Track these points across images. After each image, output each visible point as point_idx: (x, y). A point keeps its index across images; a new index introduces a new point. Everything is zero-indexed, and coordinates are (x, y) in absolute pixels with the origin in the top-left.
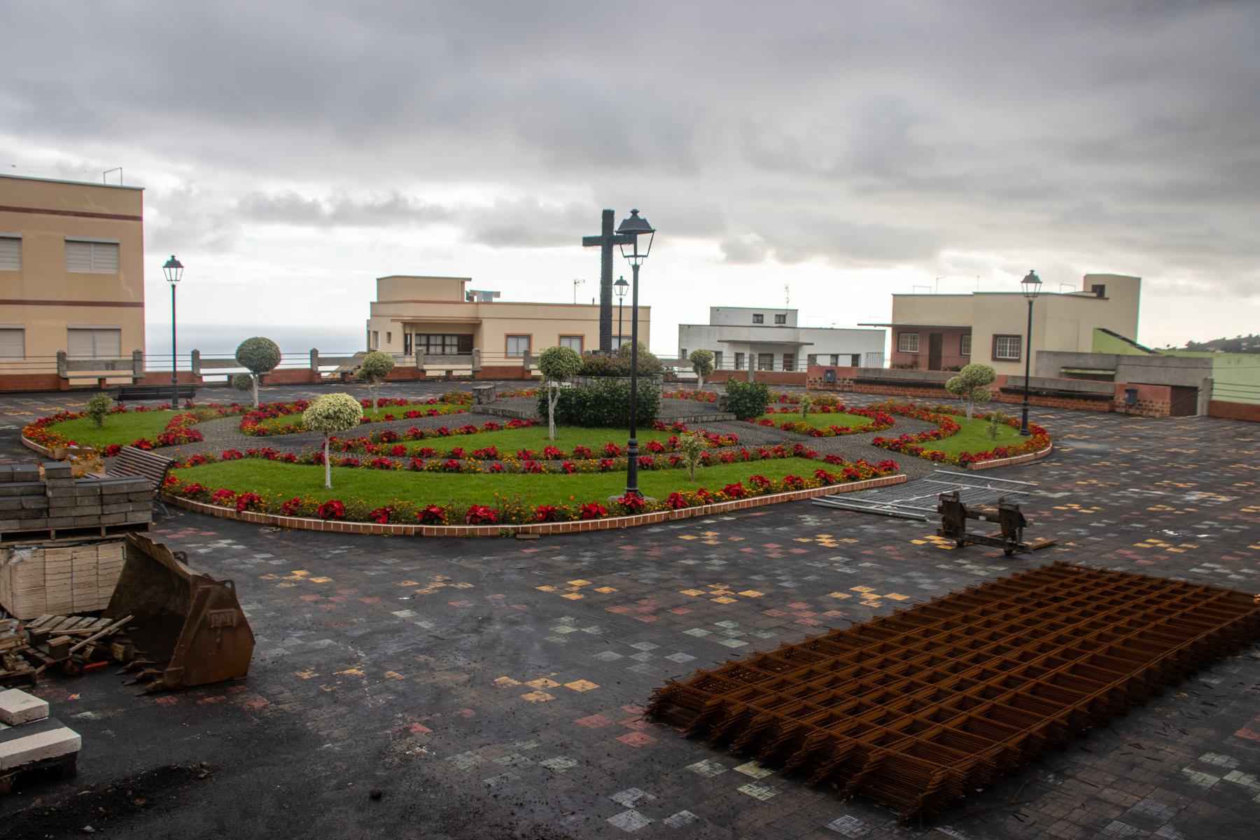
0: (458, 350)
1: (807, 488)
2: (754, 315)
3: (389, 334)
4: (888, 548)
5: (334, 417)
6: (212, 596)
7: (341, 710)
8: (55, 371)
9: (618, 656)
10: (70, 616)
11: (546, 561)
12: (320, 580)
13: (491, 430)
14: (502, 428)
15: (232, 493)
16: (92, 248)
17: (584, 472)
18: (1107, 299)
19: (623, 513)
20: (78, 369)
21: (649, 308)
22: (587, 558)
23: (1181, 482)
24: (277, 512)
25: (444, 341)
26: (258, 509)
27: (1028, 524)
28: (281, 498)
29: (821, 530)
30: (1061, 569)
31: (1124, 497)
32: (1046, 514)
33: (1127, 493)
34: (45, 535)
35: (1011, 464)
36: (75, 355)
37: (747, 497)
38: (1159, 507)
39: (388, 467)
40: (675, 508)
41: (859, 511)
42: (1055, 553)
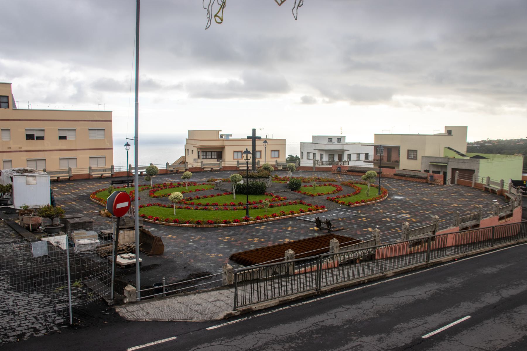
0: (217, 157)
2: (329, 139)
3: (193, 151)
5: (176, 198)
6: (158, 239)
7: (179, 258)
8: (88, 173)
9: (229, 251)
10: (131, 243)
11: (223, 233)
12: (174, 237)
13: (219, 196)
14: (222, 195)
15: (152, 217)
16: (97, 131)
18: (452, 135)
20: (95, 172)
21: (285, 140)
22: (232, 232)
24: (163, 222)
25: (212, 154)
26: (159, 221)
28: (164, 218)
34: (125, 229)
35: (365, 205)
36: (94, 167)
39: (189, 209)
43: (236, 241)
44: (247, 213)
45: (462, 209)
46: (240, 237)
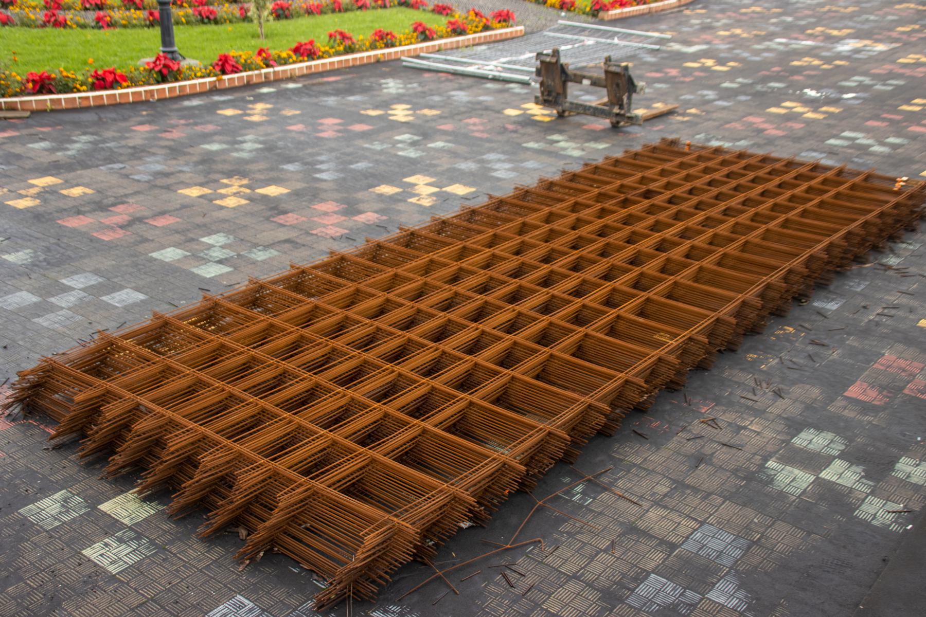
1: (400, 45)
4: (471, 121)
17: (125, 26)
19: (152, 80)
22: (81, 142)
23: (835, 28)
27: (638, 90)
29: (399, 99)
30: (670, 148)
31: (768, 50)
32: (674, 72)
33: (770, 44)
35: (650, 12)
37: (320, 58)
38: (805, 61)
40: (224, 72)
41: (455, 74)
42: (671, 124)
43: (100, 206)
44: (167, 38)
45: (431, 107)
46: (127, 176)
